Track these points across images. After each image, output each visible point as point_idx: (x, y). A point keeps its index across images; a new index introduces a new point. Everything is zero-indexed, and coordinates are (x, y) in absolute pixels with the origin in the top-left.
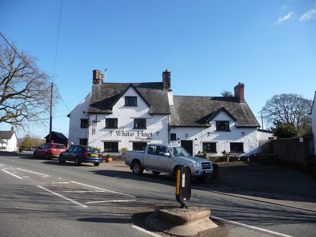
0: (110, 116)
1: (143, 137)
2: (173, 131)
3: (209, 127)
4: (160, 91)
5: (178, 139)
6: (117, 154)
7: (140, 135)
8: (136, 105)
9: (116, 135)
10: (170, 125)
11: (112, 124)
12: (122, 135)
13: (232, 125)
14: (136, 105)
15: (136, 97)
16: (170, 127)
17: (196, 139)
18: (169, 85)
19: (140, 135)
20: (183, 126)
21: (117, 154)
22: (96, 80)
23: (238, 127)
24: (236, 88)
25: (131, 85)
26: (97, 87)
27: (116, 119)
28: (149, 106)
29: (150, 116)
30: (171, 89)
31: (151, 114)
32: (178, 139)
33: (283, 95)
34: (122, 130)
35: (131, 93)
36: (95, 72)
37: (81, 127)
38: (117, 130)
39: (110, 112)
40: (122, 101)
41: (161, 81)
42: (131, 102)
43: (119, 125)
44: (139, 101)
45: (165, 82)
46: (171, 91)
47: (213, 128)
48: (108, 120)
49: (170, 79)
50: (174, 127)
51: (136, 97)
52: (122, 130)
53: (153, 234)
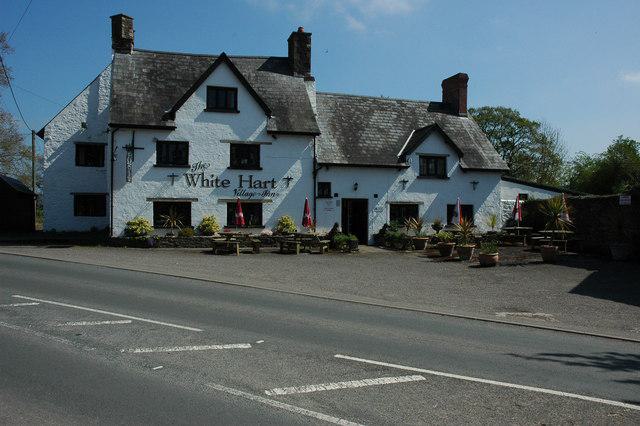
0: (172, 137)
1: (252, 190)
2: (323, 177)
3: (407, 167)
4: (285, 78)
5: (336, 195)
6: (255, 233)
7: (246, 185)
8: (235, 110)
9: (185, 184)
10: (319, 161)
11: (174, 156)
12: (199, 183)
13: (452, 168)
14: (235, 110)
15: (235, 90)
16: (317, 167)
17: (376, 196)
18: (307, 66)
19: (246, 185)
20: (370, 166)
21: (255, 233)
22: (121, 44)
23: (464, 171)
24: (446, 84)
25: (223, 59)
26: (126, 60)
27: (183, 143)
28: (268, 112)
29: (269, 139)
30: (312, 74)
31: (273, 134)
32: (336, 195)
33: (484, 109)
34: (200, 171)
35: (221, 78)
36: (117, 21)
37: (78, 164)
38: (189, 172)
39: (169, 124)
40: (197, 102)
41: (285, 54)
42: (221, 103)
43: (192, 160)
44: (243, 100)
45: (296, 57)
46: (312, 79)
47: (411, 174)
48: (161, 147)
49: (309, 50)
50: (328, 166)
51: (235, 90)
52: (200, 171)
53: (343, 422)
